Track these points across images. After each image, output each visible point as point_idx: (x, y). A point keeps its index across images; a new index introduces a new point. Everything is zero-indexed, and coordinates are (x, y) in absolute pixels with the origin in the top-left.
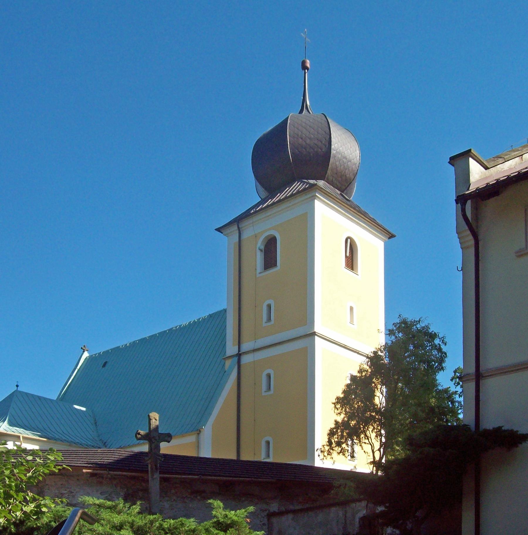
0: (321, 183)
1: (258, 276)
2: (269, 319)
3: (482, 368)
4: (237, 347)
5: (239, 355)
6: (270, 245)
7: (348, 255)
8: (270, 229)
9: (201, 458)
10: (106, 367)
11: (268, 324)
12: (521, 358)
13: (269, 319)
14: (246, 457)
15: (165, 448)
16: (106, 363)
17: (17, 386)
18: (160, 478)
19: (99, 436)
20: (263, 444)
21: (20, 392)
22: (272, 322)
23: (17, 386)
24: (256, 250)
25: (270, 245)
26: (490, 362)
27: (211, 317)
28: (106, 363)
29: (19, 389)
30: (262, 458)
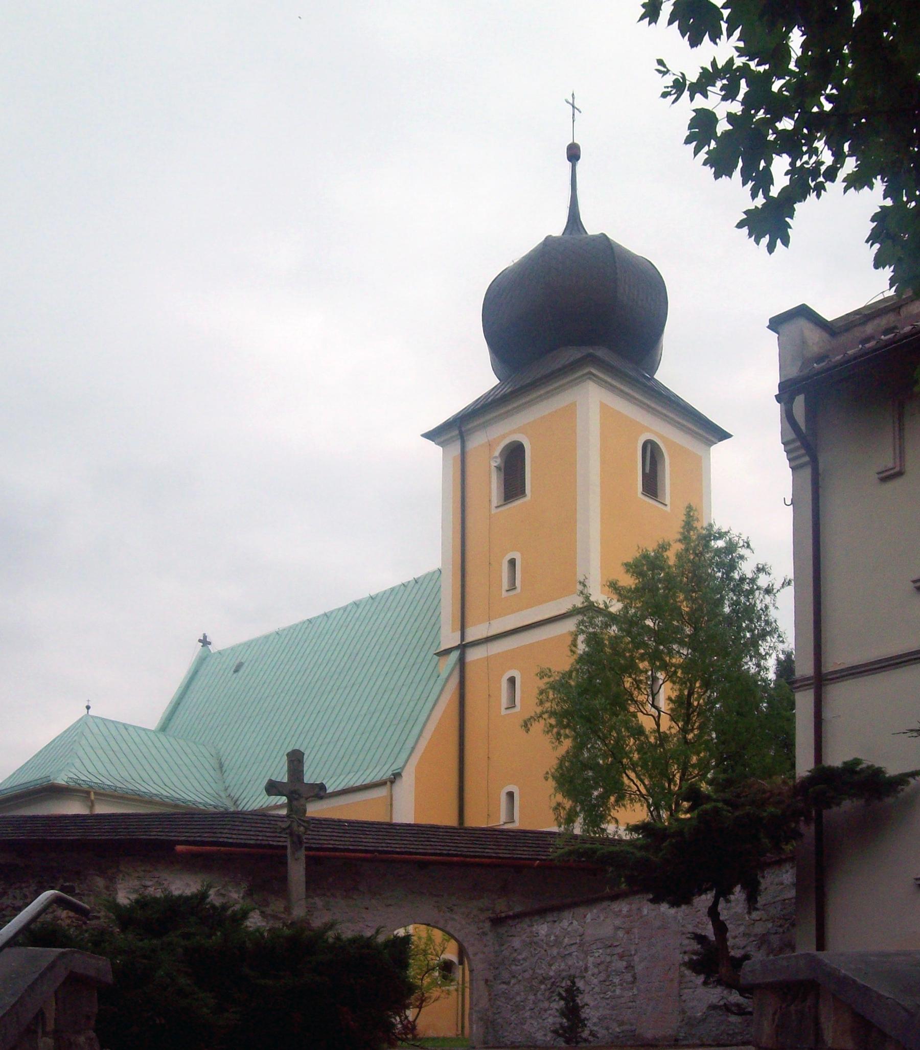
0: (600, 352)
1: (494, 511)
2: (513, 587)
3: (824, 670)
4: (458, 634)
5: (463, 647)
6: (514, 457)
7: (647, 471)
8: (514, 432)
9: (98, 815)
10: (241, 673)
11: (512, 593)
12: (914, 647)
13: (513, 587)
14: (476, 820)
15: (315, 810)
16: (236, 671)
17: (88, 708)
18: (307, 857)
19: (226, 790)
20: (503, 798)
21: (92, 717)
22: (518, 590)
23: (88, 708)
24: (490, 470)
25: (514, 457)
26: (835, 660)
27: (416, 582)
28: (236, 671)
29: (91, 712)
30: (500, 820)
